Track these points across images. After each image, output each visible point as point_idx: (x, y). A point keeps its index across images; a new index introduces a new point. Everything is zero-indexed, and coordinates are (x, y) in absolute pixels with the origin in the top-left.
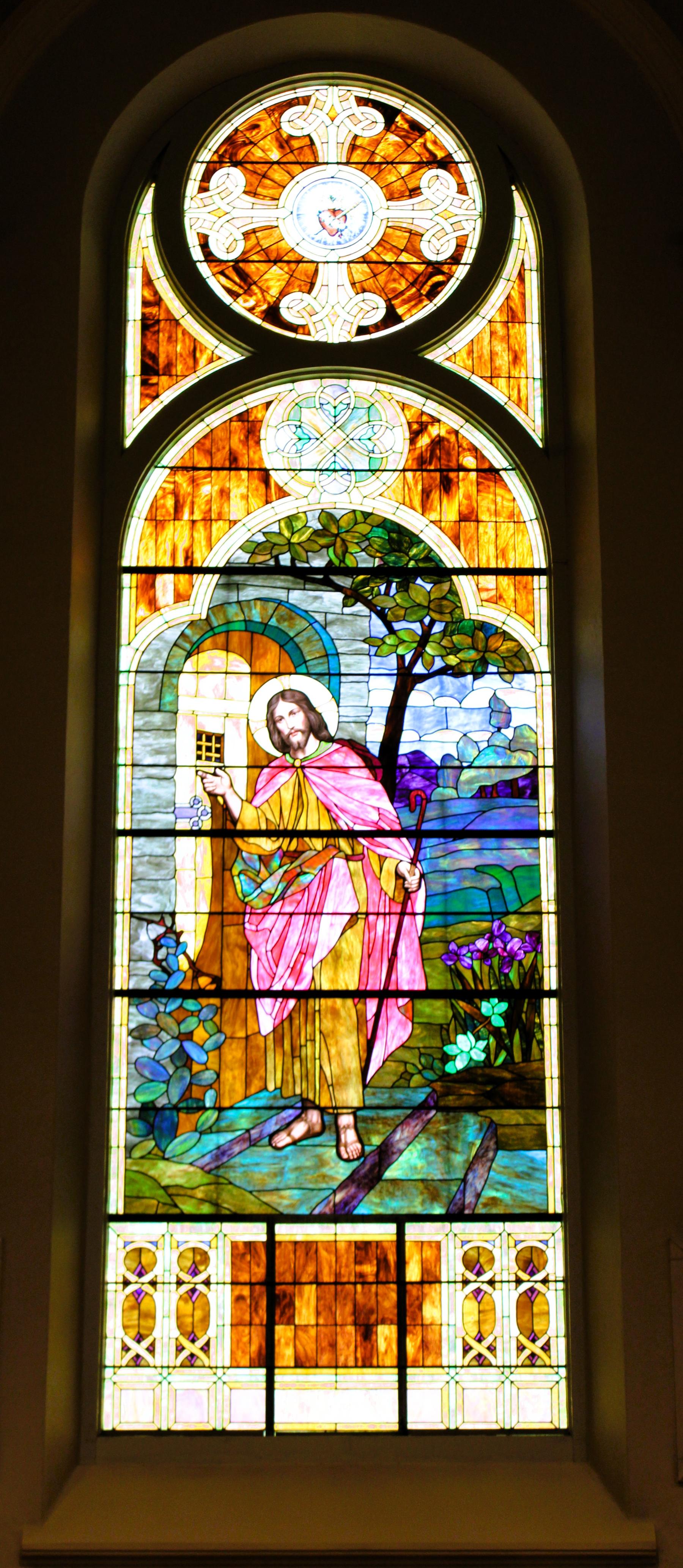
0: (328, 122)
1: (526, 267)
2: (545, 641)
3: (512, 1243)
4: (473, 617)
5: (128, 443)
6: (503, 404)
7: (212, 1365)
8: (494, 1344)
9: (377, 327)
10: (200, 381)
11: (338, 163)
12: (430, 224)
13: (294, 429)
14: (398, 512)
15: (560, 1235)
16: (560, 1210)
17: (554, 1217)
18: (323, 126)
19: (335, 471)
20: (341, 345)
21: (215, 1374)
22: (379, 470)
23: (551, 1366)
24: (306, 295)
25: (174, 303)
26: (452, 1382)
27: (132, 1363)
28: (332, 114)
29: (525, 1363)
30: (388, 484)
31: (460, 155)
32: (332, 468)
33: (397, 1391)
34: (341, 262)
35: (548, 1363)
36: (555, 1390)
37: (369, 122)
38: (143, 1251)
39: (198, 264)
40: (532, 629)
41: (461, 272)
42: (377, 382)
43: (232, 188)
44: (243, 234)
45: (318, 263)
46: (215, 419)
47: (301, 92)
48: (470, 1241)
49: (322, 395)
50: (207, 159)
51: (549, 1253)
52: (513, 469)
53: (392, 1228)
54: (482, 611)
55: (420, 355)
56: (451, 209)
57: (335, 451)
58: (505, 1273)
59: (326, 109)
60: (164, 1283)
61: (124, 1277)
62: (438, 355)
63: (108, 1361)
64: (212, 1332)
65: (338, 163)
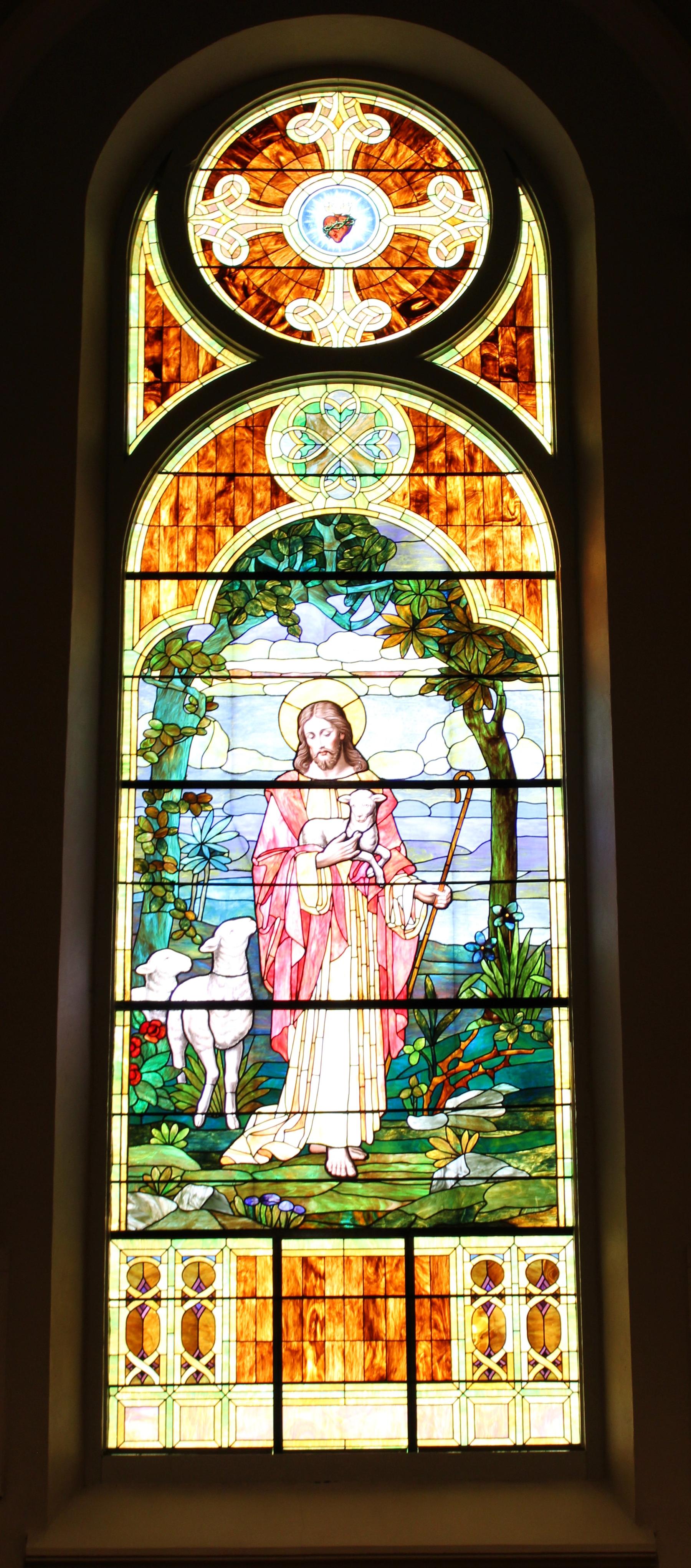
0: (333, 129)
1: (534, 271)
2: (555, 645)
4: (482, 621)
5: (131, 451)
6: (511, 408)
7: (566, 1378)
10: (204, 387)
11: (343, 171)
12: (437, 230)
13: (300, 435)
15: (572, 1244)
19: (340, 475)
22: (385, 475)
24: (311, 301)
25: (179, 311)
26: (463, 1398)
30: (393, 489)
31: (466, 163)
32: (337, 472)
33: (406, 1407)
34: (348, 269)
35: (560, 1378)
36: (163, 1407)
39: (202, 270)
40: (540, 634)
41: (469, 277)
42: (382, 386)
44: (248, 241)
46: (222, 424)
47: (307, 98)
50: (212, 167)
52: (520, 473)
54: (490, 614)
57: (340, 456)
58: (515, 1287)
60: (567, 1295)
62: (447, 360)
63: (112, 1380)
65: (343, 171)
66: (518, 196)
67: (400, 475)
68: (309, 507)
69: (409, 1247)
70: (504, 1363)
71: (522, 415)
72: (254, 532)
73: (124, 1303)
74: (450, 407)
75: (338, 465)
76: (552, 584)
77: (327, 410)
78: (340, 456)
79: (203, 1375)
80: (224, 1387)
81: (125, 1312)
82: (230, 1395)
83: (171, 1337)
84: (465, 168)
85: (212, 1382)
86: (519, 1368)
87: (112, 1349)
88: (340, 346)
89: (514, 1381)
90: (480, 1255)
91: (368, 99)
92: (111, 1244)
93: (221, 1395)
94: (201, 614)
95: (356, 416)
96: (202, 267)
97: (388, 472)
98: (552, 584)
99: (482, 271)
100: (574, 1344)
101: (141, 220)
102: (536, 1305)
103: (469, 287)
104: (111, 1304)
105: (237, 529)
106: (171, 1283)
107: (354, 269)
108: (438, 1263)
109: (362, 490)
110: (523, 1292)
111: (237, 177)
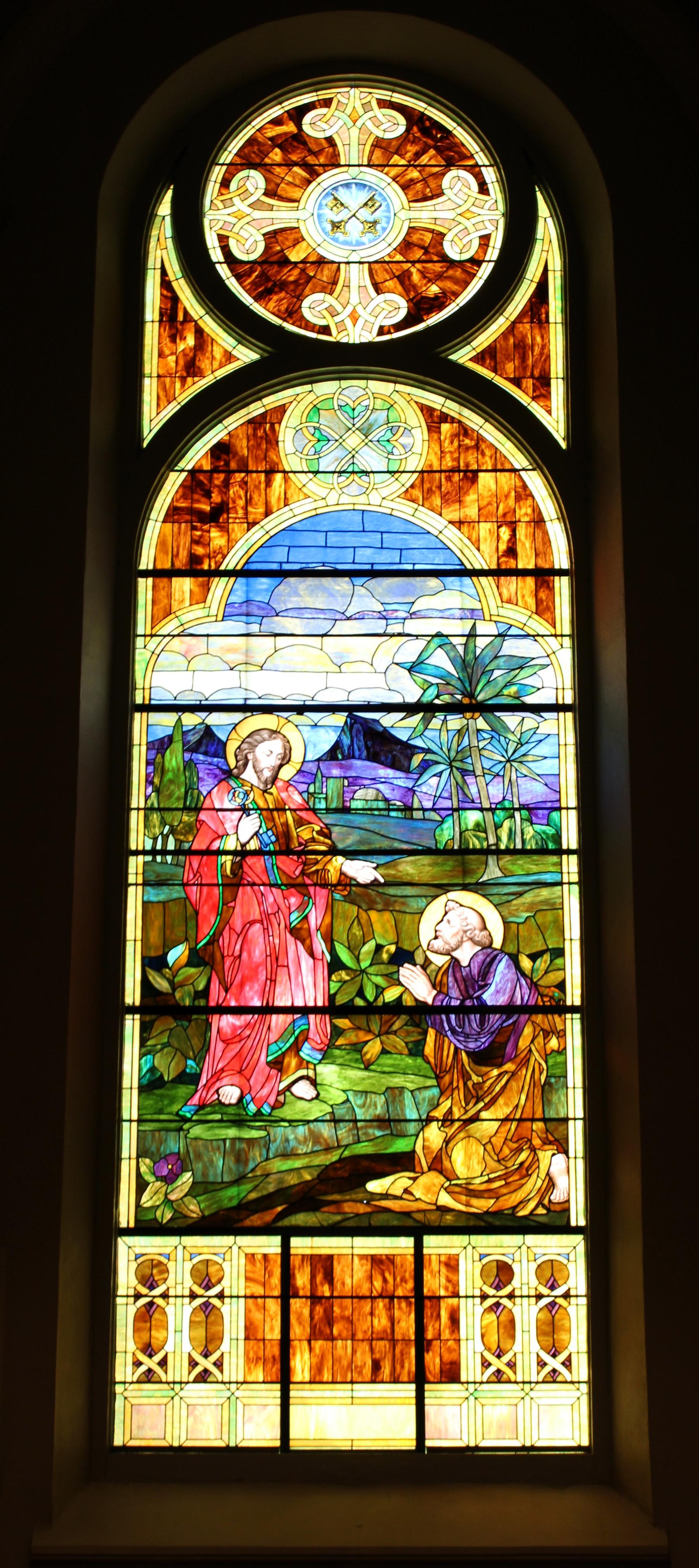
1: (550, 267)
3: (477, 1257)
5: (145, 445)
8: (513, 1360)
9: (398, 327)
11: (359, 166)
13: (312, 431)
14: (417, 514)
16: (582, 1222)
17: (577, 1230)
18: (345, 128)
19: (353, 472)
20: (362, 345)
21: (173, 1389)
22: (398, 472)
23: (222, 1382)
26: (472, 1399)
27: (494, 1378)
28: (355, 115)
29: (491, 1380)
32: (350, 469)
37: (391, 124)
38: (210, 1263)
39: (218, 266)
41: (485, 271)
43: (252, 190)
45: (339, 263)
46: (234, 421)
47: (324, 94)
48: (489, 1255)
49: (341, 397)
50: (228, 161)
51: (571, 1267)
52: (533, 470)
53: (277, 1240)
55: (443, 355)
56: (473, 209)
57: (354, 452)
58: (525, 1288)
59: (349, 111)
61: (191, 1290)
62: (463, 356)
63: (119, 1377)
64: (225, 1347)
66: (535, 192)
67: (413, 472)
68: (323, 503)
69: (419, 1246)
70: (568, 1363)
71: (536, 409)
72: (267, 528)
73: (132, 1300)
74: (463, 402)
75: (351, 461)
76: (565, 580)
77: (340, 407)
78: (354, 452)
79: (560, 1373)
80: (470, 1385)
81: (132, 1310)
82: (182, 1394)
83: (526, 1335)
84: (480, 163)
85: (569, 1380)
86: (527, 1369)
87: (120, 1345)
88: (357, 342)
89: (174, 1383)
90: (200, 1254)
91: (385, 95)
92: (119, 1240)
93: (522, 1394)
94: (213, 611)
95: (369, 412)
96: (219, 263)
97: (401, 469)
98: (565, 580)
99: (499, 263)
100: (584, 1346)
101: (156, 215)
102: (546, 1306)
103: (486, 281)
104: (119, 1300)
105: (251, 525)
106: (179, 1281)
107: (369, 263)
108: (452, 1264)
109: (376, 487)
110: (533, 1293)
111: (253, 173)
